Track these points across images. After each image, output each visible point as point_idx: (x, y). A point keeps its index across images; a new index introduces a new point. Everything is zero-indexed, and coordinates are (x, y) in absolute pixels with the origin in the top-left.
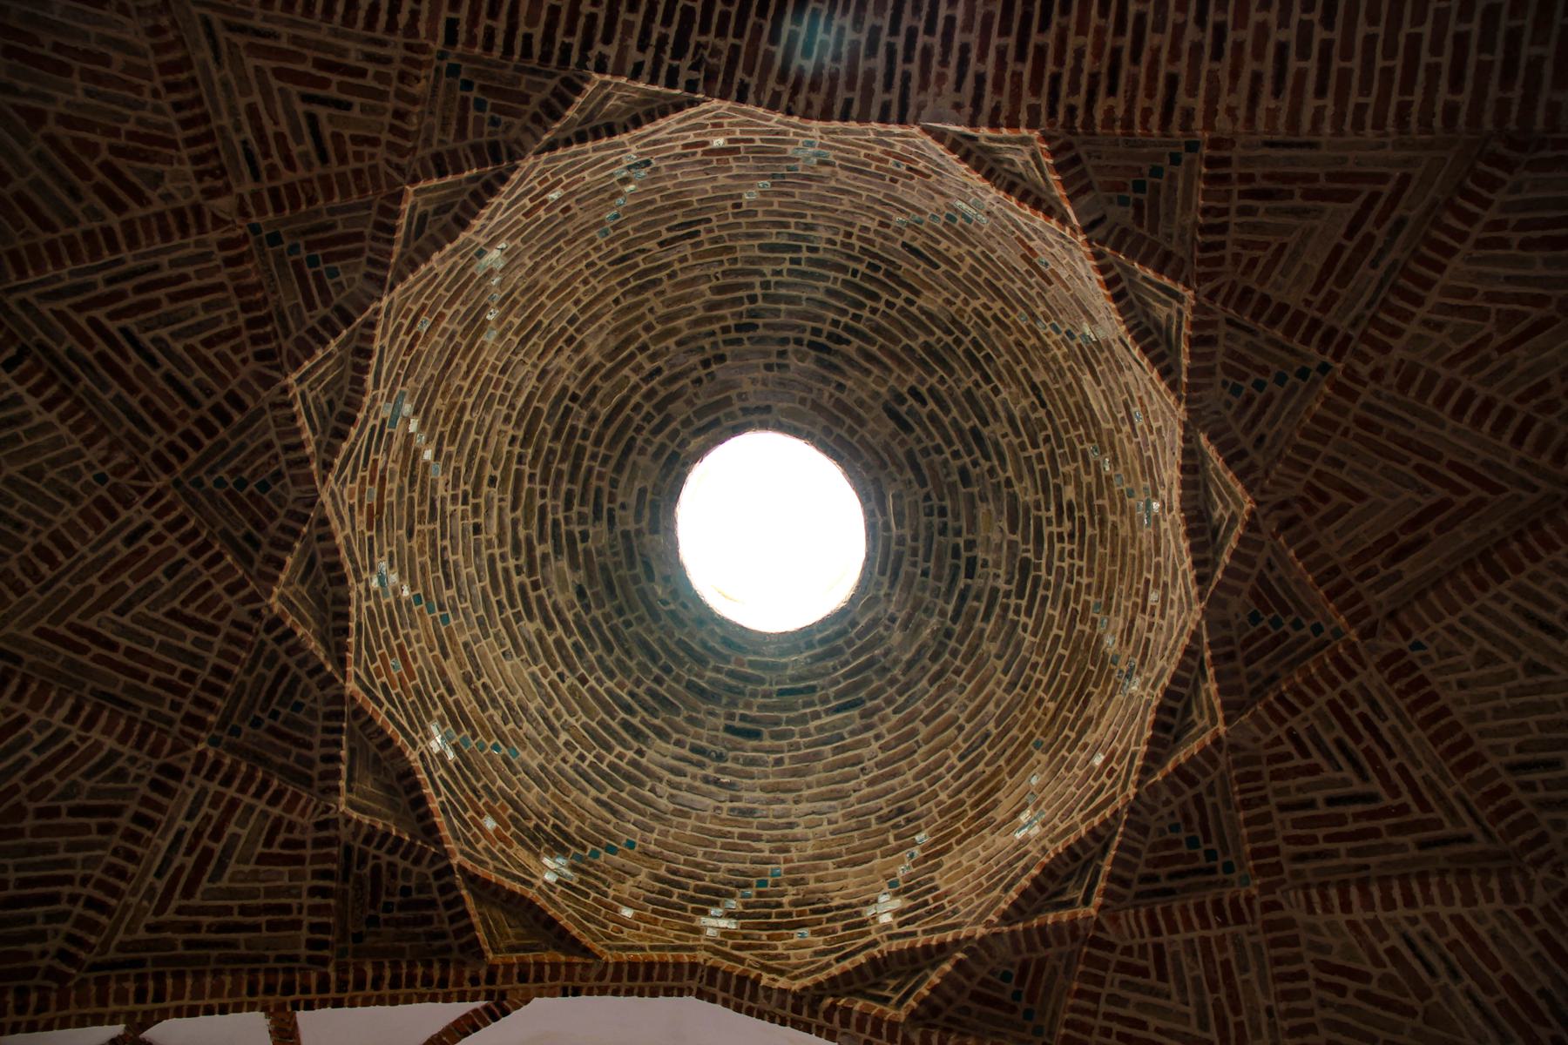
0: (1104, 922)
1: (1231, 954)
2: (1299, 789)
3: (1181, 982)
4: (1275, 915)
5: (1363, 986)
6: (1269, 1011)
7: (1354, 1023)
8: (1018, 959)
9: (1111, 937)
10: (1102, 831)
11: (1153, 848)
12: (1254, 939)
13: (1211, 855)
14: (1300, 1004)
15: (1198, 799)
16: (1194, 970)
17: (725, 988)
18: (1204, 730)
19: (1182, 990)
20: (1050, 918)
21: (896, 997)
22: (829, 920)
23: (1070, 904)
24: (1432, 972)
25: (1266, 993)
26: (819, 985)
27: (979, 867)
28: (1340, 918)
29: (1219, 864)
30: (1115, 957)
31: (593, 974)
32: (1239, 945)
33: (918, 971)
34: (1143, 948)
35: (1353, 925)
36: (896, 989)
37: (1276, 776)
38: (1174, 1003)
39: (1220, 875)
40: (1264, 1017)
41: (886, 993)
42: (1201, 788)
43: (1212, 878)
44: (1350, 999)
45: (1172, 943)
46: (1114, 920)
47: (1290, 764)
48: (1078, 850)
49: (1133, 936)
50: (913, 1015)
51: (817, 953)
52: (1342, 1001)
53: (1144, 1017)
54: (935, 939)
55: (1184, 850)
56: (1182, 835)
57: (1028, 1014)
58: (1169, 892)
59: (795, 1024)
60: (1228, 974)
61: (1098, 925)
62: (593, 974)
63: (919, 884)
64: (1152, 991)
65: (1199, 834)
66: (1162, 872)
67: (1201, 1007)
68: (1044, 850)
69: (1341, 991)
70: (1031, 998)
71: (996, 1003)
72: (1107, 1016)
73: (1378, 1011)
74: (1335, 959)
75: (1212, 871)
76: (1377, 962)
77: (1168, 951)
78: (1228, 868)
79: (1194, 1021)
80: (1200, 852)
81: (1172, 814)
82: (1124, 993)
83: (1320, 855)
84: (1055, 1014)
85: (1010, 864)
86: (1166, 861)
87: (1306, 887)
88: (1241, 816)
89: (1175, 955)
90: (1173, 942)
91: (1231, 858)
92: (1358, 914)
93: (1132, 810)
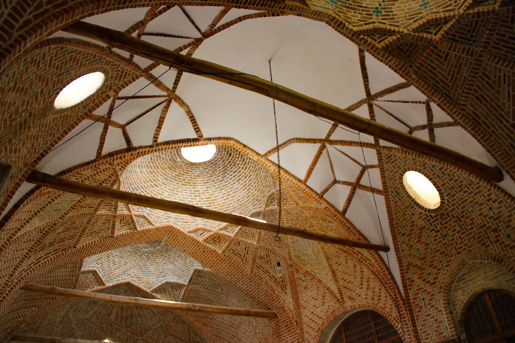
0: (439, 43)
1: (464, 62)
2: (504, 31)
3: (449, 63)
4: (480, 58)
5: (488, 80)
6: (465, 78)
7: (482, 87)
8: (411, 42)
9: (438, 46)
10: (448, 18)
11: (458, 28)
12: (472, 61)
13: (472, 36)
14: (474, 79)
15: (477, 22)
16: (453, 61)
17: (335, 23)
18: (490, 4)
19: (448, 65)
20: (425, 35)
21: (378, 40)
22: (362, 10)
23: (431, 33)
24: (504, 83)
25: (467, 74)
26: (360, 31)
27: (406, 11)
28: (494, 65)
29: (473, 39)
30: (436, 51)
31: (307, 12)
32: (467, 61)
33: (385, 35)
34: (444, 52)
35: (495, 67)
36: (379, 38)
37: (501, 25)
38: (445, 67)
39: (471, 42)
40: (463, 78)
41: (376, 38)
42: (480, 19)
43: (469, 42)
44: (484, 82)
45: (452, 53)
46: (442, 43)
47: (507, 24)
48: (439, 20)
49: (443, 48)
50: (383, 48)
51: (359, 20)
52: (482, 82)
53: (436, 68)
54: (392, 28)
55: (466, 32)
56: (467, 28)
57: (409, 56)
58: (457, 41)
59: (350, 39)
60: (461, 66)
61: (437, 43)
62: (307, 12)
63: (388, 8)
64: (441, 63)
65: (472, 30)
66: (458, 35)
67: (450, 70)
68: (428, 14)
69: (483, 79)
70: (411, 52)
71: (402, 50)
72: (428, 64)
73: (488, 87)
74: (486, 73)
75: (470, 40)
76: (495, 77)
77: (450, 55)
78: (474, 41)
79: (447, 73)
80: (469, 34)
81: (468, 22)
82: (435, 61)
83: (498, 49)
84: (416, 59)
85: (416, 14)
86: (461, 33)
87: (491, 55)
88: (487, 32)
89: (451, 57)
90: (452, 53)
91: (477, 39)
92: (498, 66)
93: (459, 17)
